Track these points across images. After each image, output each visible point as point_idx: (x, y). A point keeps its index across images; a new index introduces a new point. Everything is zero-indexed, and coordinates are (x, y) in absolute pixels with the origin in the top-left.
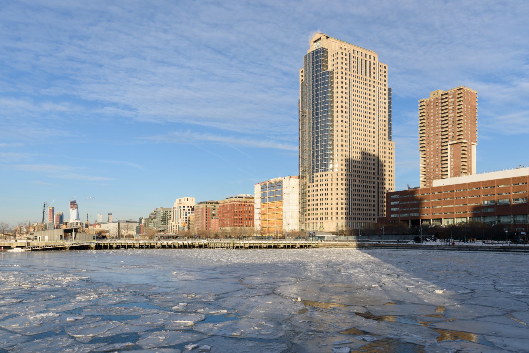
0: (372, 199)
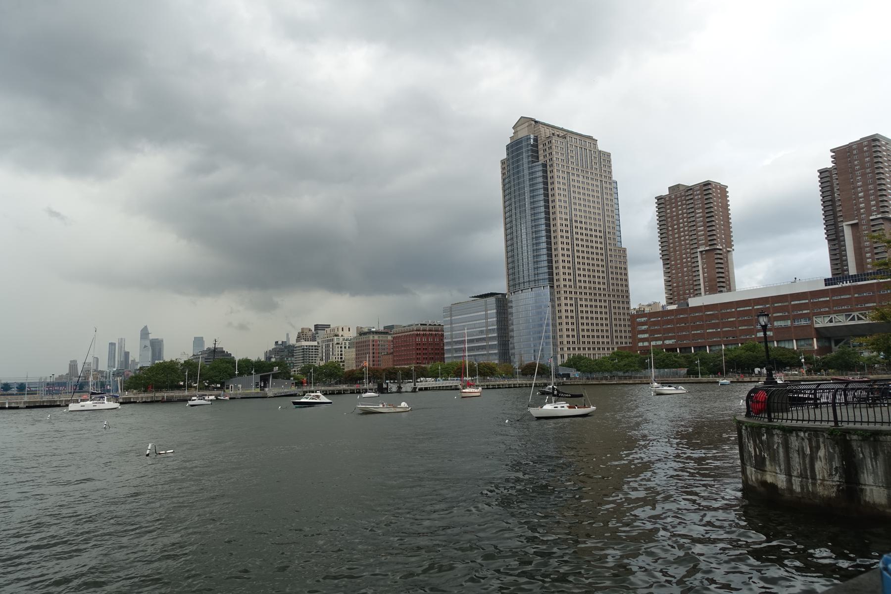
0: (604, 322)
